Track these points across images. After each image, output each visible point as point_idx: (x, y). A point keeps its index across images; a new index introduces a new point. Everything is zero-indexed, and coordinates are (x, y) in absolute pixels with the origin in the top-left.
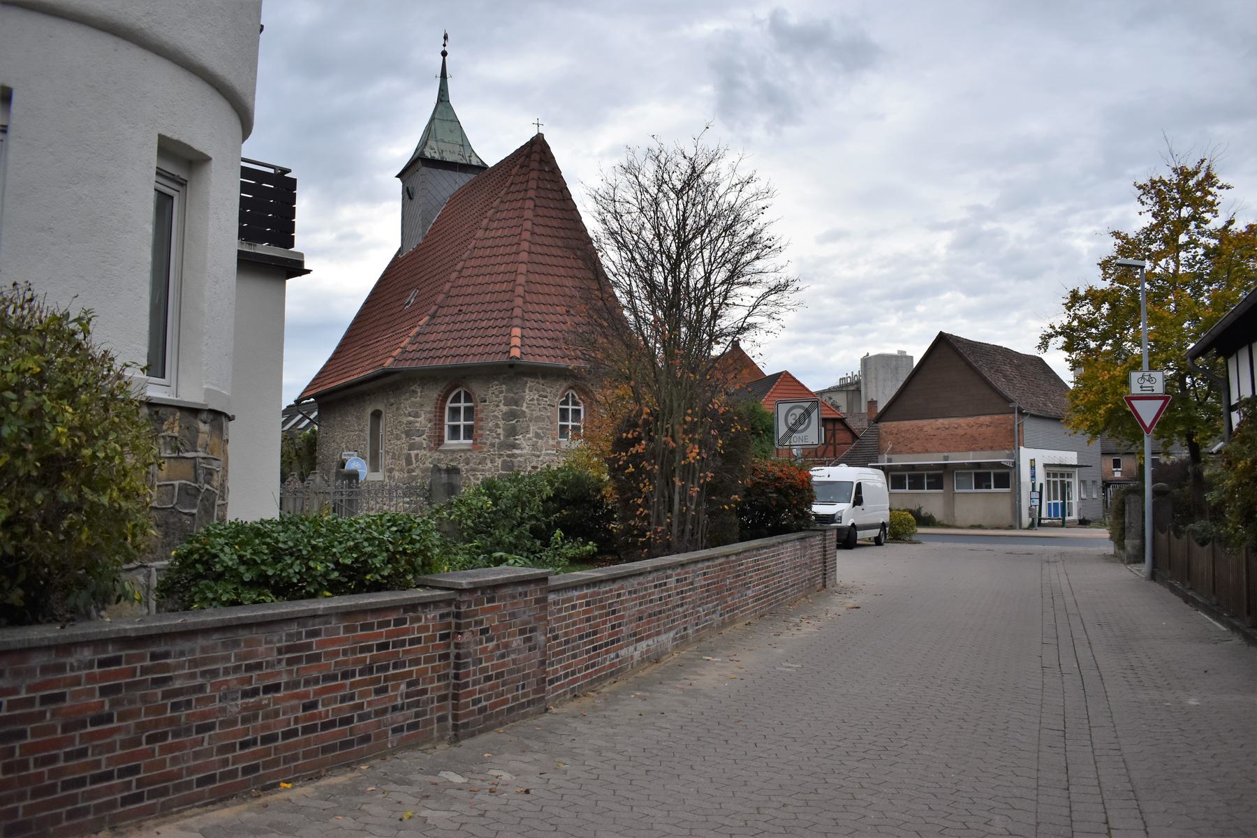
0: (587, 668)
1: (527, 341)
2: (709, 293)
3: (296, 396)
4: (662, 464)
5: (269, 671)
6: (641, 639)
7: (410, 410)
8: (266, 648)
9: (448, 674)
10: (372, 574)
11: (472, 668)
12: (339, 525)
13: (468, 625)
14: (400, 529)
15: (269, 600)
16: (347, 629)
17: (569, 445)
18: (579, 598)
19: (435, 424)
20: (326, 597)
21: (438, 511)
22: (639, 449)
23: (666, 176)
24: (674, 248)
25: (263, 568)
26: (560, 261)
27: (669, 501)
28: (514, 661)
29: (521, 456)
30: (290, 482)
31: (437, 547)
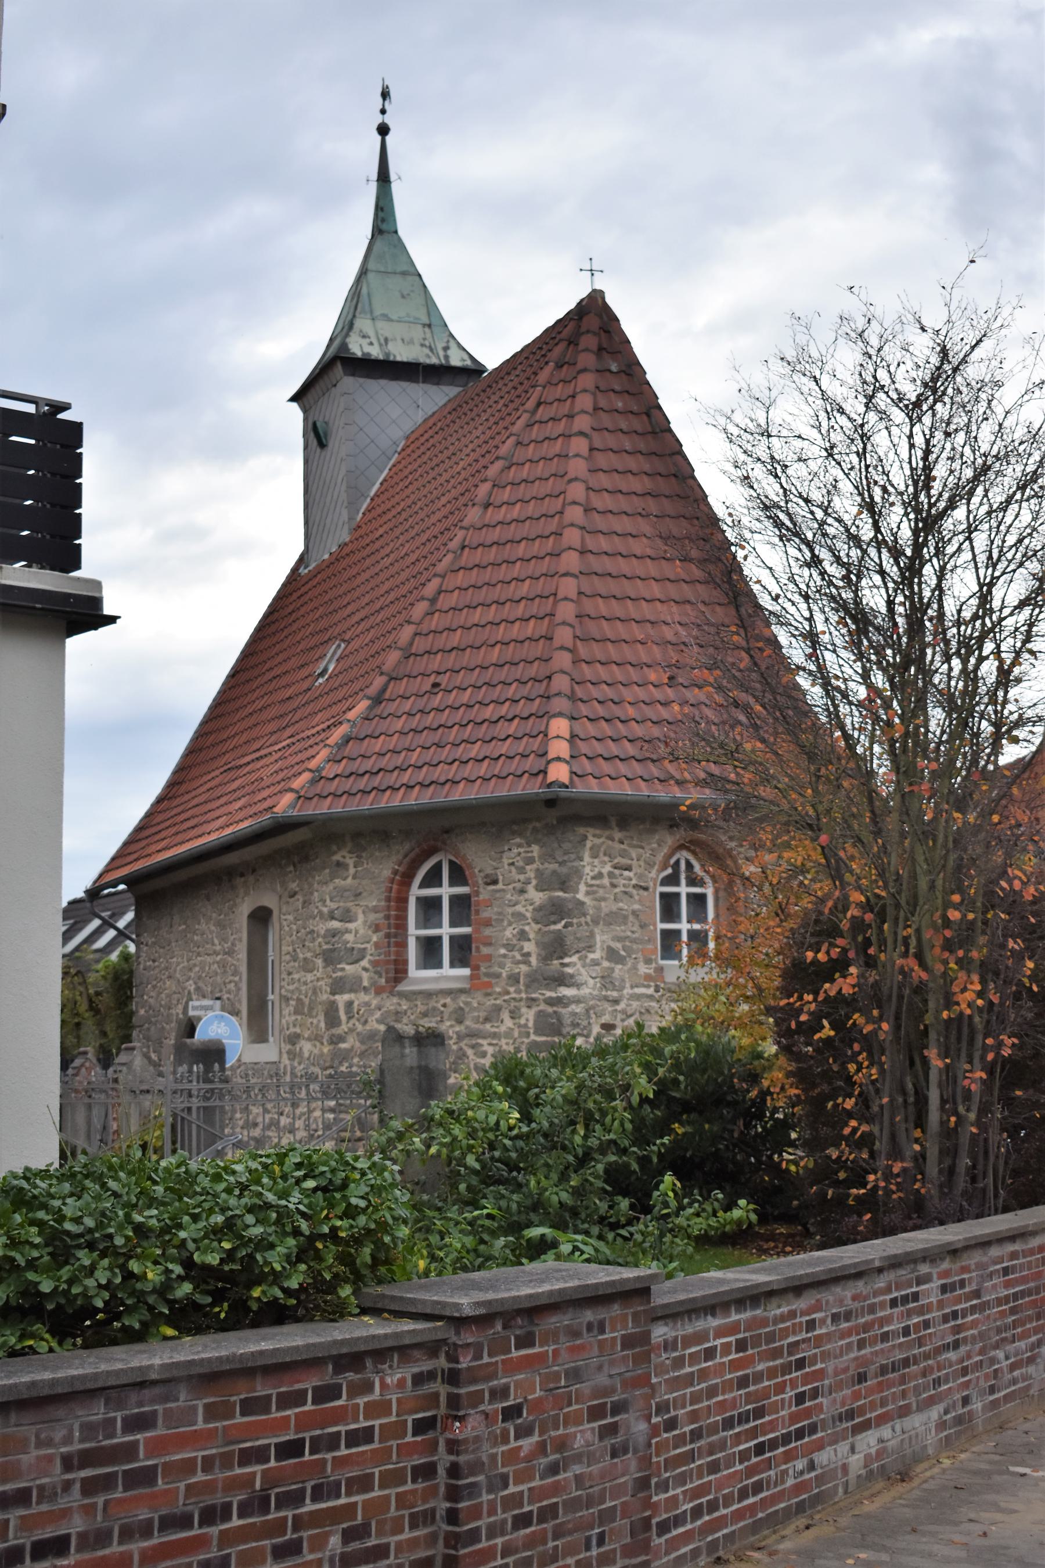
0: (743, 1494)
1: (583, 747)
2: (992, 630)
3: (87, 881)
4: (897, 1018)
5: (44, 1507)
6: (865, 1426)
7: (333, 905)
8: (38, 1458)
9: (433, 1511)
10: (264, 1287)
11: (486, 1497)
12: (191, 1178)
13: (476, 1399)
14: (324, 1183)
15: (43, 1347)
16: (212, 1413)
17: (683, 976)
18: (720, 1333)
19: (388, 936)
20: (166, 1338)
21: (400, 1136)
22: (845, 985)
23: (883, 376)
24: (906, 533)
25: (31, 1276)
26: (652, 569)
27: (917, 1102)
28: (579, 1479)
29: (578, 1001)
30: (79, 1068)
31: (405, 1222)
